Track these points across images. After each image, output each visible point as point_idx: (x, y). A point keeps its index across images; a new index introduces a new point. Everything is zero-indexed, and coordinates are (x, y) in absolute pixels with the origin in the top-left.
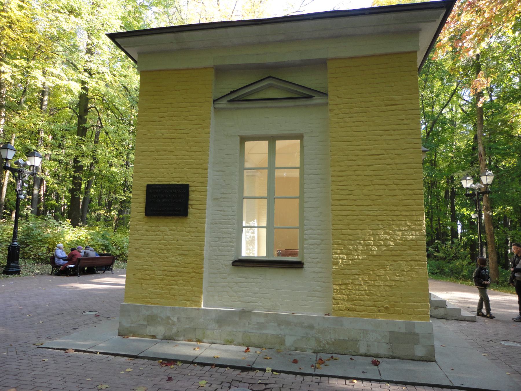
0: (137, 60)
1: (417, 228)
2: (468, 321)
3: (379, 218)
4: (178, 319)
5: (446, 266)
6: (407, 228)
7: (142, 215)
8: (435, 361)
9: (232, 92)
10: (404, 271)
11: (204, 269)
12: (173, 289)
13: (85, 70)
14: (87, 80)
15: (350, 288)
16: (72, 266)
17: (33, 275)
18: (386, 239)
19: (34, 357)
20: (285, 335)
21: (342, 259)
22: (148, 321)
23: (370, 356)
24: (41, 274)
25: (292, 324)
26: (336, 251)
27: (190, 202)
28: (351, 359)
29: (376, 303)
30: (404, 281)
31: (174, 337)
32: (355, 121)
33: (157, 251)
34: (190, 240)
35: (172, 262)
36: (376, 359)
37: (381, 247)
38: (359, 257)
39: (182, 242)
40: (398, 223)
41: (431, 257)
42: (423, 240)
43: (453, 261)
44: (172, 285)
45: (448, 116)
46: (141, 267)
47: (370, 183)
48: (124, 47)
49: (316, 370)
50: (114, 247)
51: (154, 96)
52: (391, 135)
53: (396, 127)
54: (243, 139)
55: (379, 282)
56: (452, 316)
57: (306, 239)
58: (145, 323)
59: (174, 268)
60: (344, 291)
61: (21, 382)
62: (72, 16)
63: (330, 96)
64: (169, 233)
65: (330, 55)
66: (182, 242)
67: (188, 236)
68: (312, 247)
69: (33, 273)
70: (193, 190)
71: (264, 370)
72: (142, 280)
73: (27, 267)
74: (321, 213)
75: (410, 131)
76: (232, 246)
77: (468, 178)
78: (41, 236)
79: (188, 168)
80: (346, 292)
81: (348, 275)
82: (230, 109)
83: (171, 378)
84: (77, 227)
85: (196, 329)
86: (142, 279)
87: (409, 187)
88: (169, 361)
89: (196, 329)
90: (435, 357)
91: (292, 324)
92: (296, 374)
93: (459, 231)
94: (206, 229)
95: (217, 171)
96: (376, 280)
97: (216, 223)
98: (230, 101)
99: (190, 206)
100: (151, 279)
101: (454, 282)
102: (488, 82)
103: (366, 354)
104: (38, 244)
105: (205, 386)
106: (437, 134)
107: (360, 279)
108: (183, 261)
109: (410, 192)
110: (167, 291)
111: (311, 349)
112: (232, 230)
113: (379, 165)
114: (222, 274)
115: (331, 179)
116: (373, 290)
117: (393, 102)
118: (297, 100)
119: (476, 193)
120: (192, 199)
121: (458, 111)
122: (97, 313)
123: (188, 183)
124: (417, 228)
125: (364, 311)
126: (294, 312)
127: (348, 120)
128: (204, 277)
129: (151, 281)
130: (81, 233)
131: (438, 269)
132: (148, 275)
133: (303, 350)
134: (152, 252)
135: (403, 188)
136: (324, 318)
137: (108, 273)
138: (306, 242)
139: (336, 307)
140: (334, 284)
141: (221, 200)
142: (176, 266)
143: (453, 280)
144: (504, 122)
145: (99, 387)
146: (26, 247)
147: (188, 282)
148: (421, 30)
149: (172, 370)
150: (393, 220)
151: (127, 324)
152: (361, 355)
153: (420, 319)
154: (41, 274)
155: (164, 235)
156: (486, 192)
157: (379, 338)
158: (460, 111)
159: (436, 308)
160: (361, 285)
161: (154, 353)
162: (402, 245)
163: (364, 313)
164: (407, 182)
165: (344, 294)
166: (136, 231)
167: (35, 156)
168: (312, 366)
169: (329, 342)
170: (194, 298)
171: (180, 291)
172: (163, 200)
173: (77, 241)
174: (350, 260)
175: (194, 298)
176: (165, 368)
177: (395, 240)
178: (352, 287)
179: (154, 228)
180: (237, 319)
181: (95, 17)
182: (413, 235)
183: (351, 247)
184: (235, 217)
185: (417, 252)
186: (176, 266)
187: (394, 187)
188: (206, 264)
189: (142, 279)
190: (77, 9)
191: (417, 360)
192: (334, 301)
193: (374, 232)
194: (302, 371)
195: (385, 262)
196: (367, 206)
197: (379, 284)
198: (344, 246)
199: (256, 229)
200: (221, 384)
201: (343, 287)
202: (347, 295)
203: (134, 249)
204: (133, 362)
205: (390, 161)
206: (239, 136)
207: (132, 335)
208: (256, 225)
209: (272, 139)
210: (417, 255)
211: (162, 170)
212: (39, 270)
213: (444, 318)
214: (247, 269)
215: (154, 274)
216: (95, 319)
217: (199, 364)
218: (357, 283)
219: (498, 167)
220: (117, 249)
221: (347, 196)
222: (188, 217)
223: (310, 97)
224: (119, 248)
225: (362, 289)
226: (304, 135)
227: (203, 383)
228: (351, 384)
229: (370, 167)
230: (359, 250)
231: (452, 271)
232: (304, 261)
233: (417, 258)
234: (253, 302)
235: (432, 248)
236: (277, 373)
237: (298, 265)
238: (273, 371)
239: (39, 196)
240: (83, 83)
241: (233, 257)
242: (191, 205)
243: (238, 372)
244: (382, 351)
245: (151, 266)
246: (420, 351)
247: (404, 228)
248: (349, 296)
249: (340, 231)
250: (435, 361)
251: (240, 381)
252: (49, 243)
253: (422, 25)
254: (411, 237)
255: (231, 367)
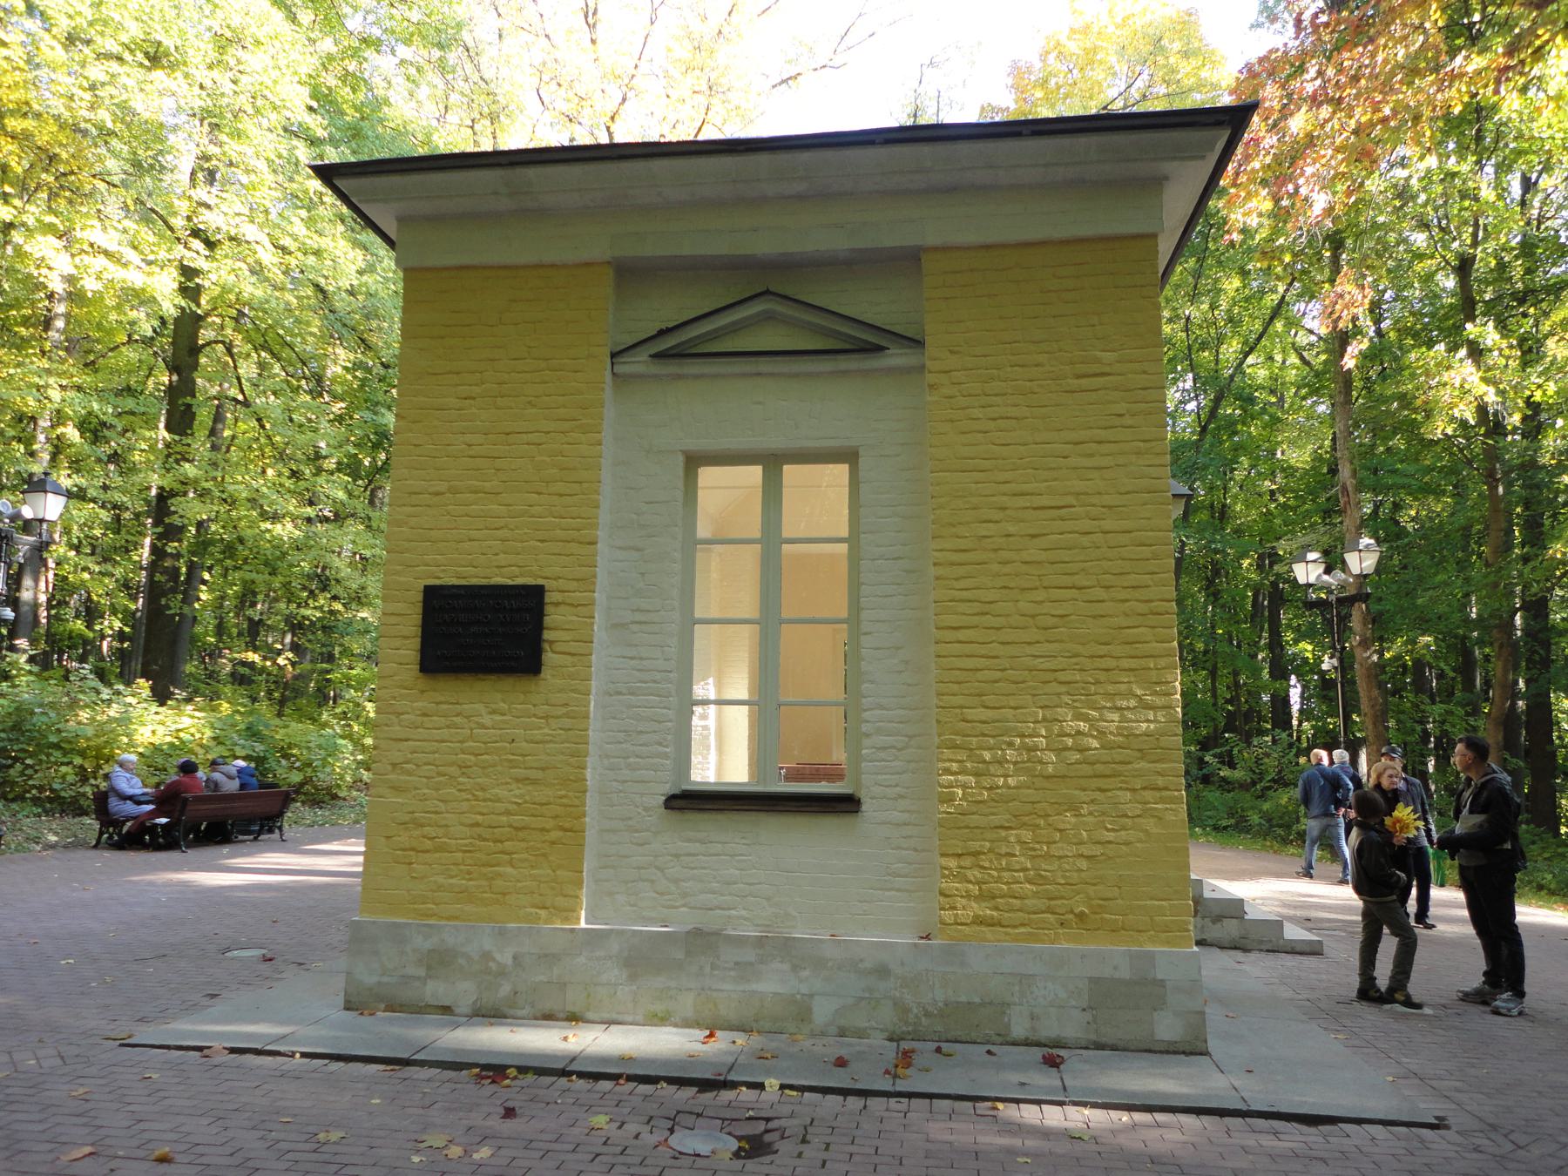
0: (393, 237)
1: (1159, 701)
2: (1301, 953)
3: (1062, 676)
4: (515, 958)
5: (1252, 808)
6: (1133, 703)
7: (411, 669)
8: (1205, 1053)
9: (662, 333)
10: (1126, 816)
11: (587, 819)
12: (500, 875)
13: (196, 233)
14: (200, 263)
15: (987, 864)
16: (164, 820)
17: (38, 848)
18: (1079, 733)
19: (115, 1069)
20: (811, 996)
21: (964, 787)
22: (429, 968)
23: (1038, 1044)
24: (65, 847)
25: (830, 964)
26: (947, 764)
27: (547, 635)
28: (989, 1052)
29: (1052, 903)
30: (1127, 844)
31: (506, 1010)
32: (997, 415)
33: (453, 770)
34: (549, 738)
35: (499, 800)
36: (1055, 1051)
37: (1067, 753)
38: (1010, 780)
39: (524, 744)
40: (1111, 688)
41: (1213, 783)
42: (1176, 735)
43: (1271, 793)
44: (498, 865)
45: (1262, 374)
46: (407, 818)
47: (1038, 583)
48: (360, 201)
49: (898, 1081)
50: (284, 762)
51: (442, 338)
52: (1091, 455)
53: (1102, 434)
54: (694, 461)
55: (1062, 849)
56: (1261, 942)
57: (868, 736)
58: (422, 972)
59: (504, 819)
60: (969, 873)
61: (103, 1132)
62: (158, 75)
63: (931, 349)
64: (487, 720)
65: (931, 239)
66: (524, 744)
67: (540, 728)
68: (882, 755)
69: (37, 843)
70: (553, 600)
71: (760, 1086)
72: (412, 853)
73: (18, 826)
74: (907, 662)
75: (1141, 444)
76: (666, 756)
77: (1312, 556)
78: (59, 731)
79: (542, 541)
80: (976, 874)
81: (979, 831)
82: (656, 377)
83: (513, 1109)
84: (169, 702)
85: (565, 984)
86: (413, 849)
87: (1137, 594)
88: (494, 1070)
89: (565, 984)
90: (1206, 1041)
91: (830, 964)
92: (845, 1092)
93: (1295, 708)
94: (592, 709)
95: (620, 548)
96: (1055, 842)
97: (619, 693)
98: (657, 356)
99: (546, 646)
100: (441, 848)
101: (1275, 852)
102: (1364, 297)
103: (1027, 1039)
104: (48, 755)
105: (606, 1127)
106: (1231, 426)
107: (1012, 839)
108: (527, 798)
109: (1142, 608)
110: (484, 883)
111: (882, 1030)
112: (665, 711)
113: (1061, 534)
114: (637, 831)
115: (932, 571)
116: (1047, 867)
117: (1095, 368)
118: (839, 357)
119: (1333, 598)
120: (552, 626)
121: (1287, 363)
122: (264, 951)
123: (540, 582)
124: (1159, 701)
125: (1023, 925)
126: (832, 932)
127: (977, 413)
128: (587, 840)
129: (437, 855)
130: (185, 722)
131: (1231, 815)
132: (429, 839)
133: (861, 1034)
134: (440, 774)
135: (1123, 595)
136: (915, 945)
137: (269, 840)
138: (866, 742)
139: (947, 916)
140: (942, 855)
141: (635, 627)
142: (508, 813)
143: (1272, 847)
144: (1405, 400)
145: (322, 1136)
146: (11, 766)
147: (544, 855)
148: (1166, 178)
149: (513, 1091)
150: (1097, 682)
151: (368, 977)
152: (1014, 1044)
153: (1168, 943)
154: (65, 847)
155: (473, 726)
156: (1362, 597)
157: (1063, 995)
158: (1293, 359)
159: (1218, 919)
160: (1014, 855)
161: (456, 1051)
162: (1120, 747)
163: (1022, 930)
164: (1132, 579)
165: (970, 882)
166: (393, 717)
167: (46, 492)
168: (887, 1072)
169: (930, 1009)
170: (560, 901)
171: (519, 881)
172: (473, 630)
173: (171, 745)
174: (984, 788)
175: (560, 901)
176: (489, 1088)
177: (1102, 734)
178: (991, 861)
179: (445, 706)
180: (680, 955)
181: (230, 74)
182: (1148, 721)
183: (987, 756)
184: (671, 675)
185: (1160, 766)
186: (508, 813)
187: (1100, 593)
188: (591, 803)
189: (413, 849)
190: (172, 50)
191: (1161, 1052)
192: (941, 899)
193: (1048, 713)
194: (859, 1086)
195: (1077, 792)
196: (1029, 643)
197: (1061, 853)
198: (968, 753)
199: (712, 709)
200: (648, 1122)
201: (967, 861)
202: (978, 883)
203: (389, 768)
204: (399, 1074)
205: (1087, 525)
206: (684, 452)
207: (383, 1006)
208: (712, 697)
209: (772, 462)
210: (1159, 773)
211: (467, 545)
212: (56, 834)
213: (1238, 946)
214: (706, 816)
215: (445, 836)
216: (265, 968)
217: (582, 1075)
218: (1004, 850)
219: (1397, 523)
220: (292, 768)
221: (976, 618)
222: (542, 675)
223: (879, 349)
224: (298, 764)
225: (1018, 867)
226: (861, 452)
227: (600, 1120)
228: (991, 1113)
229: (1036, 541)
230: (1008, 762)
231: (1269, 820)
232: (863, 795)
233: (1160, 782)
234: (723, 909)
235: (1214, 756)
236: (795, 1093)
237: (846, 804)
238: (782, 1087)
239: (35, 605)
240: (188, 272)
241: (668, 786)
242: (551, 643)
243: (690, 1091)
244: (1072, 1027)
245: (436, 813)
246: (1167, 1028)
247: (1125, 704)
248: (984, 887)
249: (958, 711)
250: (1205, 1053)
251: (698, 1115)
252: (82, 753)
253: (1168, 167)
254: (1144, 725)
255: (671, 1081)
